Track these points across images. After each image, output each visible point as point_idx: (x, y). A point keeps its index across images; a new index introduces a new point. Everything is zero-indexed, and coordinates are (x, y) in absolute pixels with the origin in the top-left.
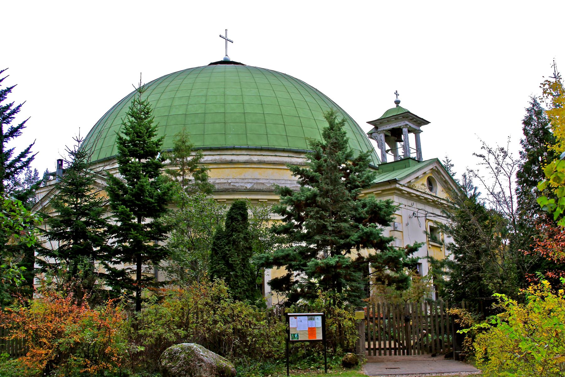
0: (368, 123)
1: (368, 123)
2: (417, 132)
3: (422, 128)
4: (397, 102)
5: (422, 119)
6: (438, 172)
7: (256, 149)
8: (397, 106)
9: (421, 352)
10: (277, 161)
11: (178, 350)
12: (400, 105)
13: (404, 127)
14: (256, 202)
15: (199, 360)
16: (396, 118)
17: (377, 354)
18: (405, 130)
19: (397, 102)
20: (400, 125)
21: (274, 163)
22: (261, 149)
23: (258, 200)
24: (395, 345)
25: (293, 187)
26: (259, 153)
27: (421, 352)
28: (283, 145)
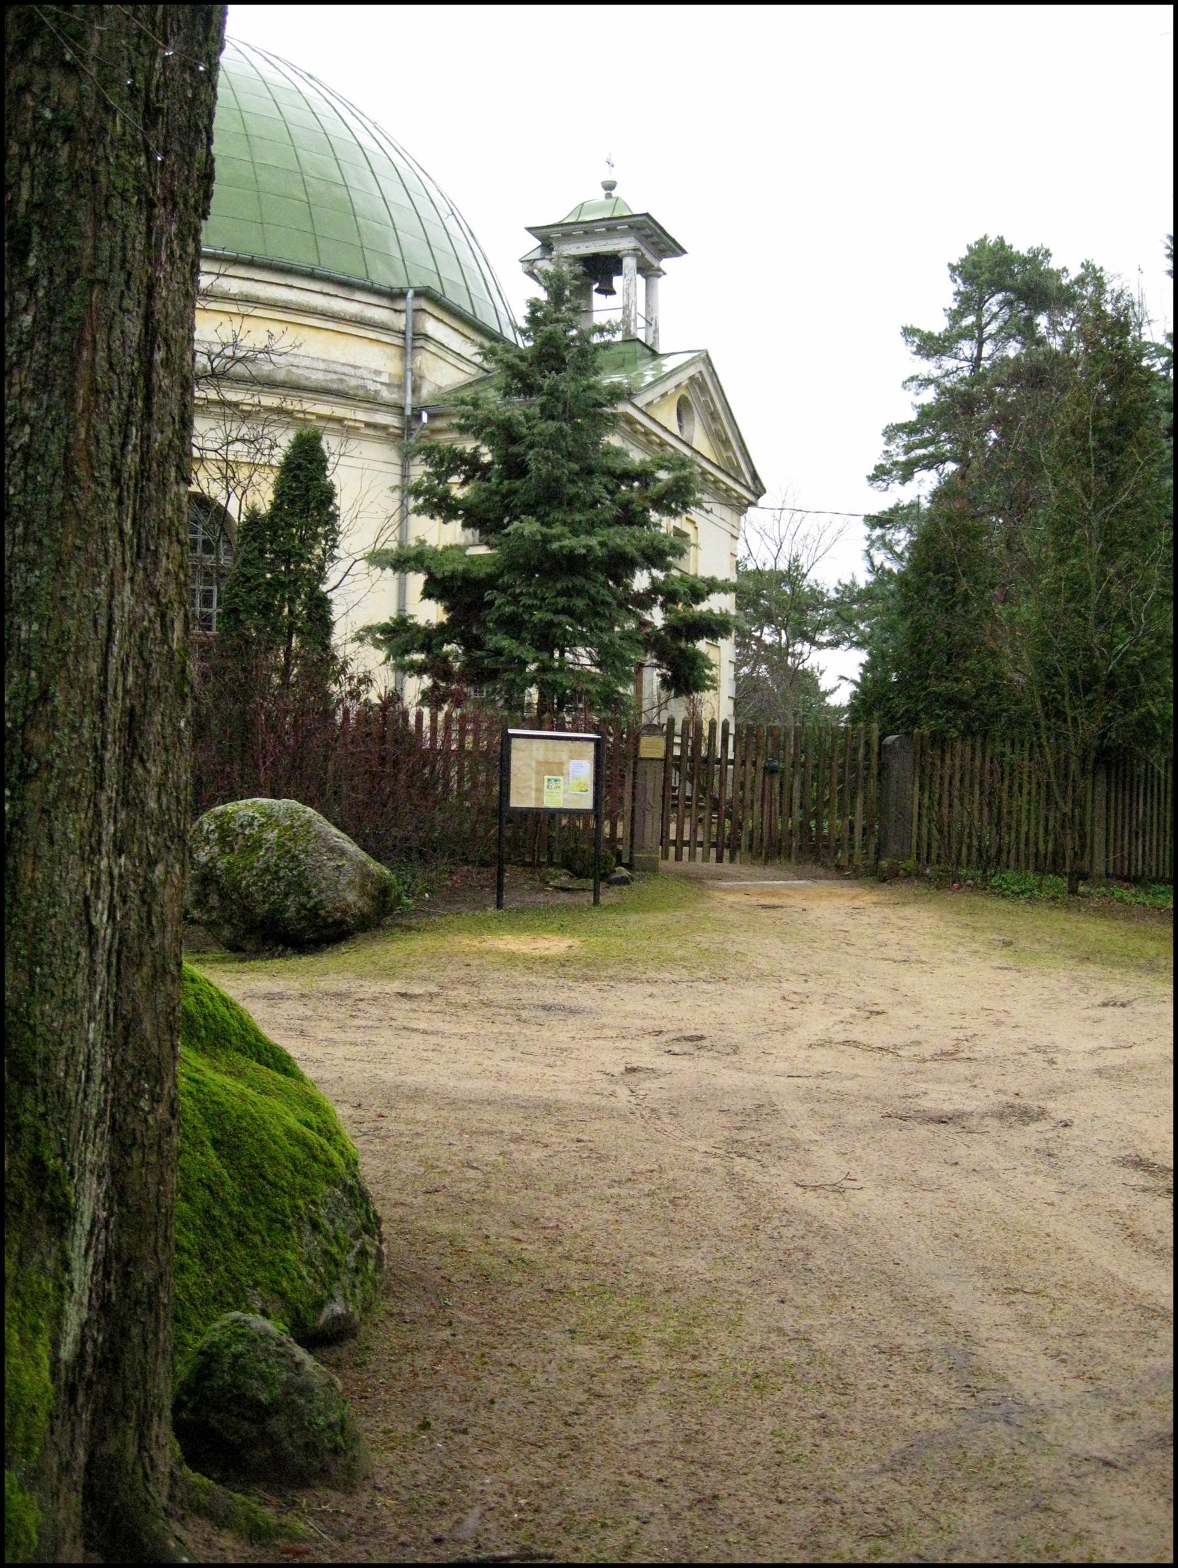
0: (529, 229)
1: (529, 229)
2: (647, 271)
3: (666, 264)
4: (609, 187)
5: (673, 241)
6: (703, 388)
7: (236, 261)
8: (609, 196)
9: (726, 853)
10: (292, 302)
11: (253, 818)
12: (614, 193)
13: (628, 255)
14: (336, 426)
15: (331, 849)
16: (612, 226)
17: (699, 856)
18: (629, 263)
19: (609, 187)
20: (617, 248)
21: (286, 307)
22: (251, 264)
23: (340, 420)
24: (694, 832)
25: (332, 381)
26: (242, 272)
27: (726, 853)
28: (303, 257)
